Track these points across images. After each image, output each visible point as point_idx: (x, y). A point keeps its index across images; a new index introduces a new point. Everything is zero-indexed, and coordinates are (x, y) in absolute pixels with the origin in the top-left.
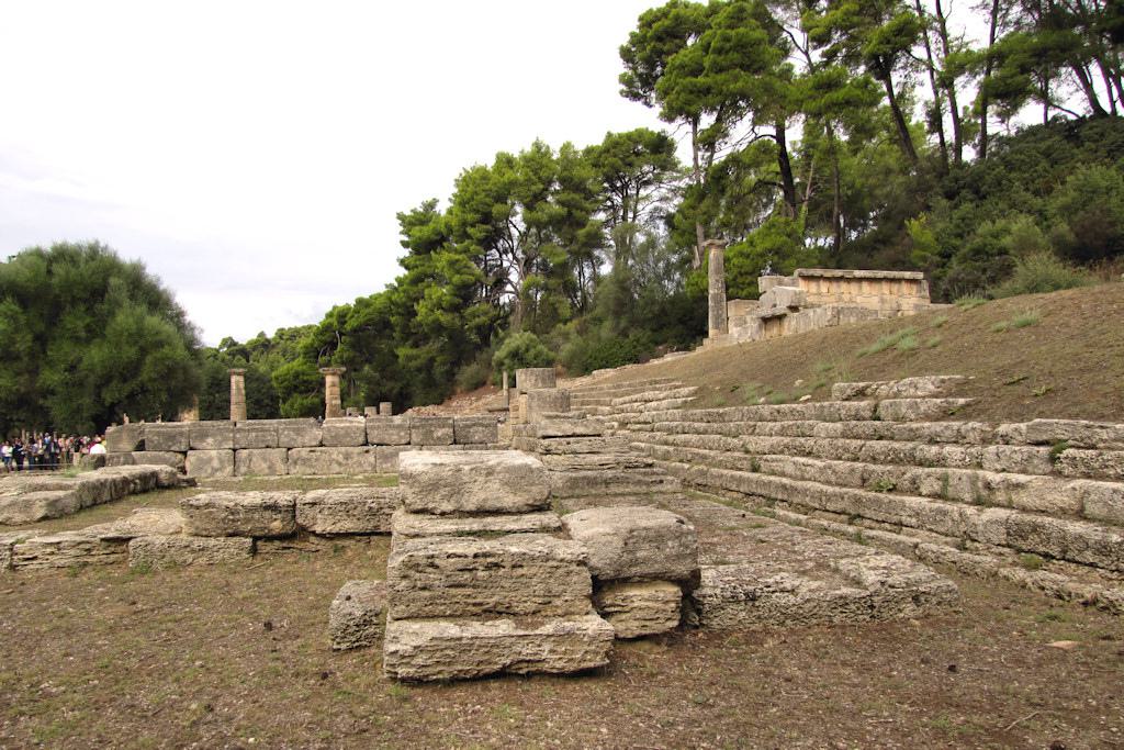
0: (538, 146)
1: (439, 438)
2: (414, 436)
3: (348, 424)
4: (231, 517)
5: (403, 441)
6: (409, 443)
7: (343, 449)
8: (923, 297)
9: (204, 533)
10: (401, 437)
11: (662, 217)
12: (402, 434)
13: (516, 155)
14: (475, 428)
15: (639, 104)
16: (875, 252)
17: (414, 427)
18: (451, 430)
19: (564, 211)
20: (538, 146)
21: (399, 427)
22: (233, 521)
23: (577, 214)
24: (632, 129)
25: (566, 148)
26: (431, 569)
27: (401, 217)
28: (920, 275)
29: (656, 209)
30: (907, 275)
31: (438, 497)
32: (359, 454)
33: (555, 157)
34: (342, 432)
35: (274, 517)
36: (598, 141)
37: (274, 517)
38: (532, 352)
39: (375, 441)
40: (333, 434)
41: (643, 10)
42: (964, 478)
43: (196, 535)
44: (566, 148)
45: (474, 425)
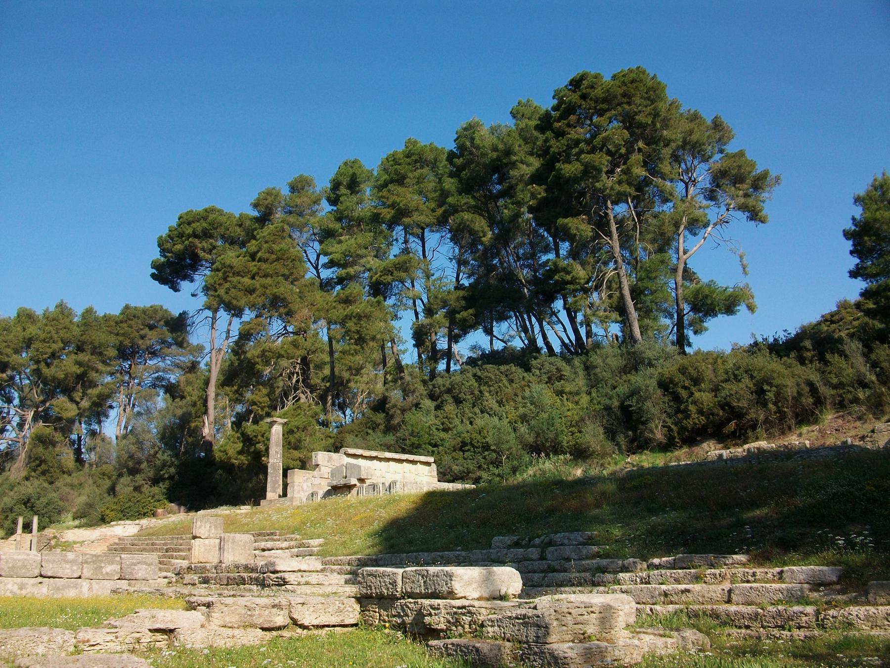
0: (61, 306)
1: (107, 573)
2: (85, 571)
3: (25, 557)
4: (249, 613)
5: (76, 575)
6: (80, 577)
7: (19, 580)
8: (433, 477)
9: (230, 625)
10: (73, 571)
11: (163, 386)
12: (75, 568)
13: (39, 312)
14: (140, 566)
15: (165, 288)
16: (51, 413)
17: (86, 562)
18: (119, 567)
19: (79, 370)
20: (61, 306)
21: (73, 562)
22: (250, 615)
23: (93, 375)
24: (148, 305)
25: (89, 311)
26: (568, 615)
27: (62, 301)
28: (431, 459)
29: (158, 378)
30: (423, 458)
31: (471, 589)
32: (33, 585)
33: (76, 320)
34: (19, 564)
35: (278, 613)
36: (115, 310)
37: (278, 613)
38: (44, 500)
39: (49, 574)
40: (10, 565)
41: (183, 210)
42: (645, 590)
43: (225, 626)
44: (89, 311)
45: (139, 563)
